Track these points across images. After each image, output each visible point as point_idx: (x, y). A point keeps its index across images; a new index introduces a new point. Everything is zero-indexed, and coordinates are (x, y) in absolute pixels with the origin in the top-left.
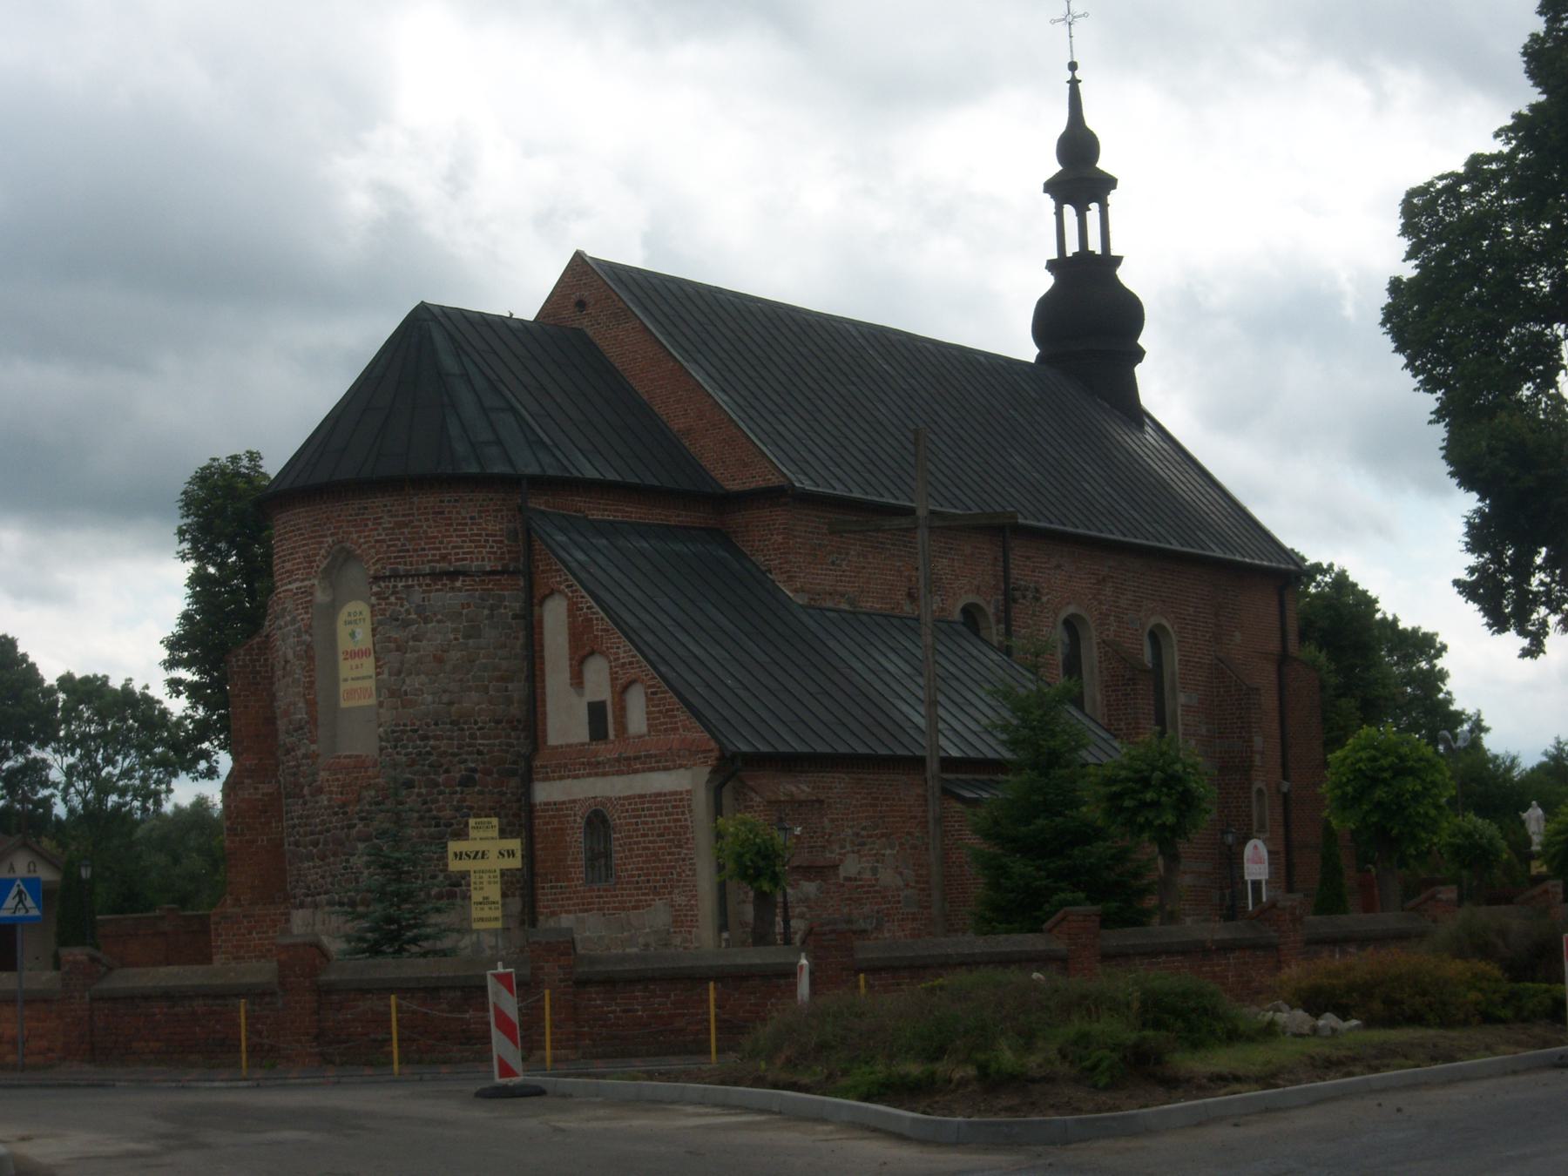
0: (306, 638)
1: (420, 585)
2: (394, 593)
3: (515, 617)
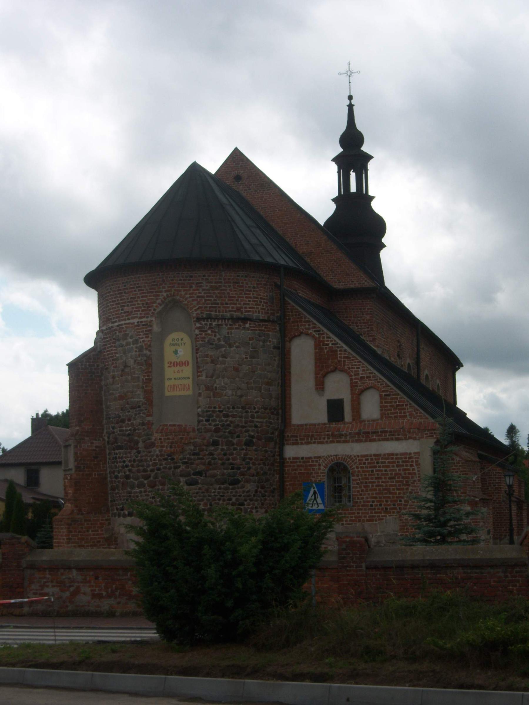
0: (147, 352)
1: (226, 325)
2: (210, 328)
3: (275, 347)
